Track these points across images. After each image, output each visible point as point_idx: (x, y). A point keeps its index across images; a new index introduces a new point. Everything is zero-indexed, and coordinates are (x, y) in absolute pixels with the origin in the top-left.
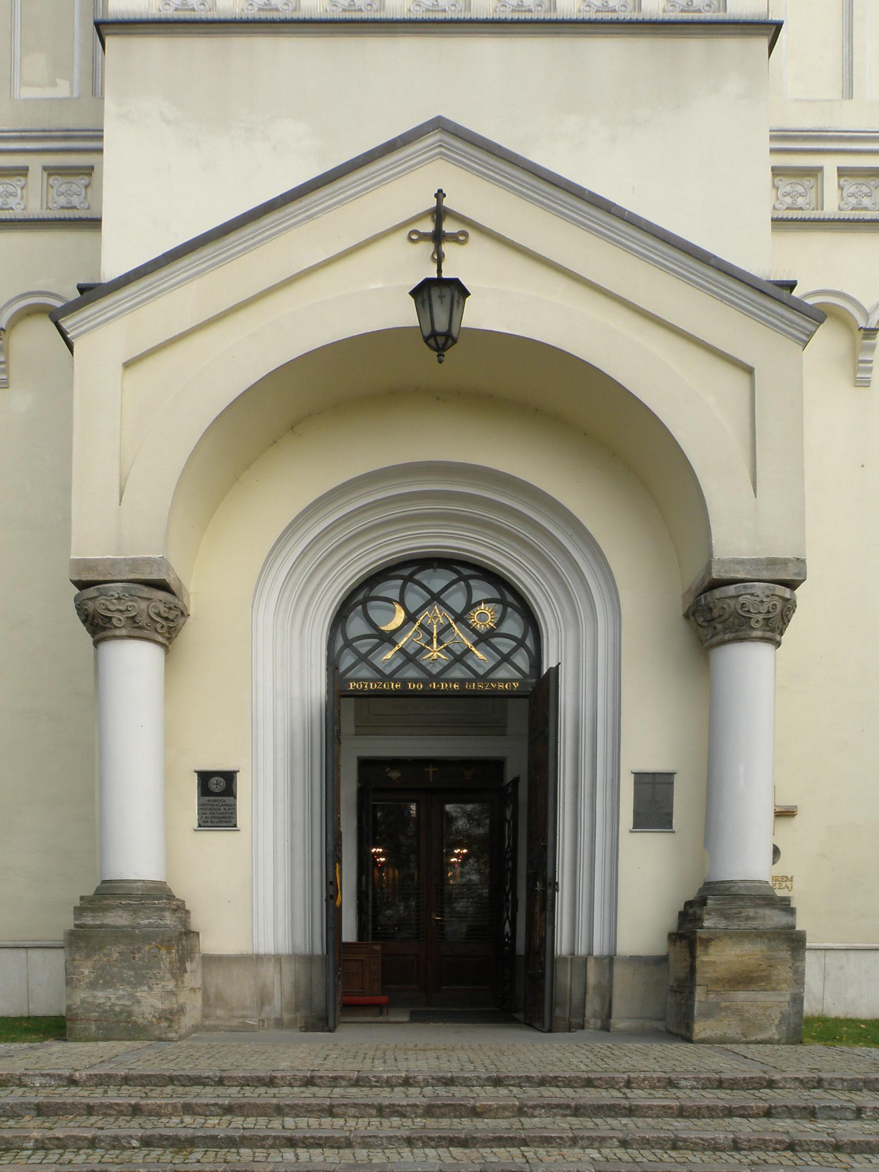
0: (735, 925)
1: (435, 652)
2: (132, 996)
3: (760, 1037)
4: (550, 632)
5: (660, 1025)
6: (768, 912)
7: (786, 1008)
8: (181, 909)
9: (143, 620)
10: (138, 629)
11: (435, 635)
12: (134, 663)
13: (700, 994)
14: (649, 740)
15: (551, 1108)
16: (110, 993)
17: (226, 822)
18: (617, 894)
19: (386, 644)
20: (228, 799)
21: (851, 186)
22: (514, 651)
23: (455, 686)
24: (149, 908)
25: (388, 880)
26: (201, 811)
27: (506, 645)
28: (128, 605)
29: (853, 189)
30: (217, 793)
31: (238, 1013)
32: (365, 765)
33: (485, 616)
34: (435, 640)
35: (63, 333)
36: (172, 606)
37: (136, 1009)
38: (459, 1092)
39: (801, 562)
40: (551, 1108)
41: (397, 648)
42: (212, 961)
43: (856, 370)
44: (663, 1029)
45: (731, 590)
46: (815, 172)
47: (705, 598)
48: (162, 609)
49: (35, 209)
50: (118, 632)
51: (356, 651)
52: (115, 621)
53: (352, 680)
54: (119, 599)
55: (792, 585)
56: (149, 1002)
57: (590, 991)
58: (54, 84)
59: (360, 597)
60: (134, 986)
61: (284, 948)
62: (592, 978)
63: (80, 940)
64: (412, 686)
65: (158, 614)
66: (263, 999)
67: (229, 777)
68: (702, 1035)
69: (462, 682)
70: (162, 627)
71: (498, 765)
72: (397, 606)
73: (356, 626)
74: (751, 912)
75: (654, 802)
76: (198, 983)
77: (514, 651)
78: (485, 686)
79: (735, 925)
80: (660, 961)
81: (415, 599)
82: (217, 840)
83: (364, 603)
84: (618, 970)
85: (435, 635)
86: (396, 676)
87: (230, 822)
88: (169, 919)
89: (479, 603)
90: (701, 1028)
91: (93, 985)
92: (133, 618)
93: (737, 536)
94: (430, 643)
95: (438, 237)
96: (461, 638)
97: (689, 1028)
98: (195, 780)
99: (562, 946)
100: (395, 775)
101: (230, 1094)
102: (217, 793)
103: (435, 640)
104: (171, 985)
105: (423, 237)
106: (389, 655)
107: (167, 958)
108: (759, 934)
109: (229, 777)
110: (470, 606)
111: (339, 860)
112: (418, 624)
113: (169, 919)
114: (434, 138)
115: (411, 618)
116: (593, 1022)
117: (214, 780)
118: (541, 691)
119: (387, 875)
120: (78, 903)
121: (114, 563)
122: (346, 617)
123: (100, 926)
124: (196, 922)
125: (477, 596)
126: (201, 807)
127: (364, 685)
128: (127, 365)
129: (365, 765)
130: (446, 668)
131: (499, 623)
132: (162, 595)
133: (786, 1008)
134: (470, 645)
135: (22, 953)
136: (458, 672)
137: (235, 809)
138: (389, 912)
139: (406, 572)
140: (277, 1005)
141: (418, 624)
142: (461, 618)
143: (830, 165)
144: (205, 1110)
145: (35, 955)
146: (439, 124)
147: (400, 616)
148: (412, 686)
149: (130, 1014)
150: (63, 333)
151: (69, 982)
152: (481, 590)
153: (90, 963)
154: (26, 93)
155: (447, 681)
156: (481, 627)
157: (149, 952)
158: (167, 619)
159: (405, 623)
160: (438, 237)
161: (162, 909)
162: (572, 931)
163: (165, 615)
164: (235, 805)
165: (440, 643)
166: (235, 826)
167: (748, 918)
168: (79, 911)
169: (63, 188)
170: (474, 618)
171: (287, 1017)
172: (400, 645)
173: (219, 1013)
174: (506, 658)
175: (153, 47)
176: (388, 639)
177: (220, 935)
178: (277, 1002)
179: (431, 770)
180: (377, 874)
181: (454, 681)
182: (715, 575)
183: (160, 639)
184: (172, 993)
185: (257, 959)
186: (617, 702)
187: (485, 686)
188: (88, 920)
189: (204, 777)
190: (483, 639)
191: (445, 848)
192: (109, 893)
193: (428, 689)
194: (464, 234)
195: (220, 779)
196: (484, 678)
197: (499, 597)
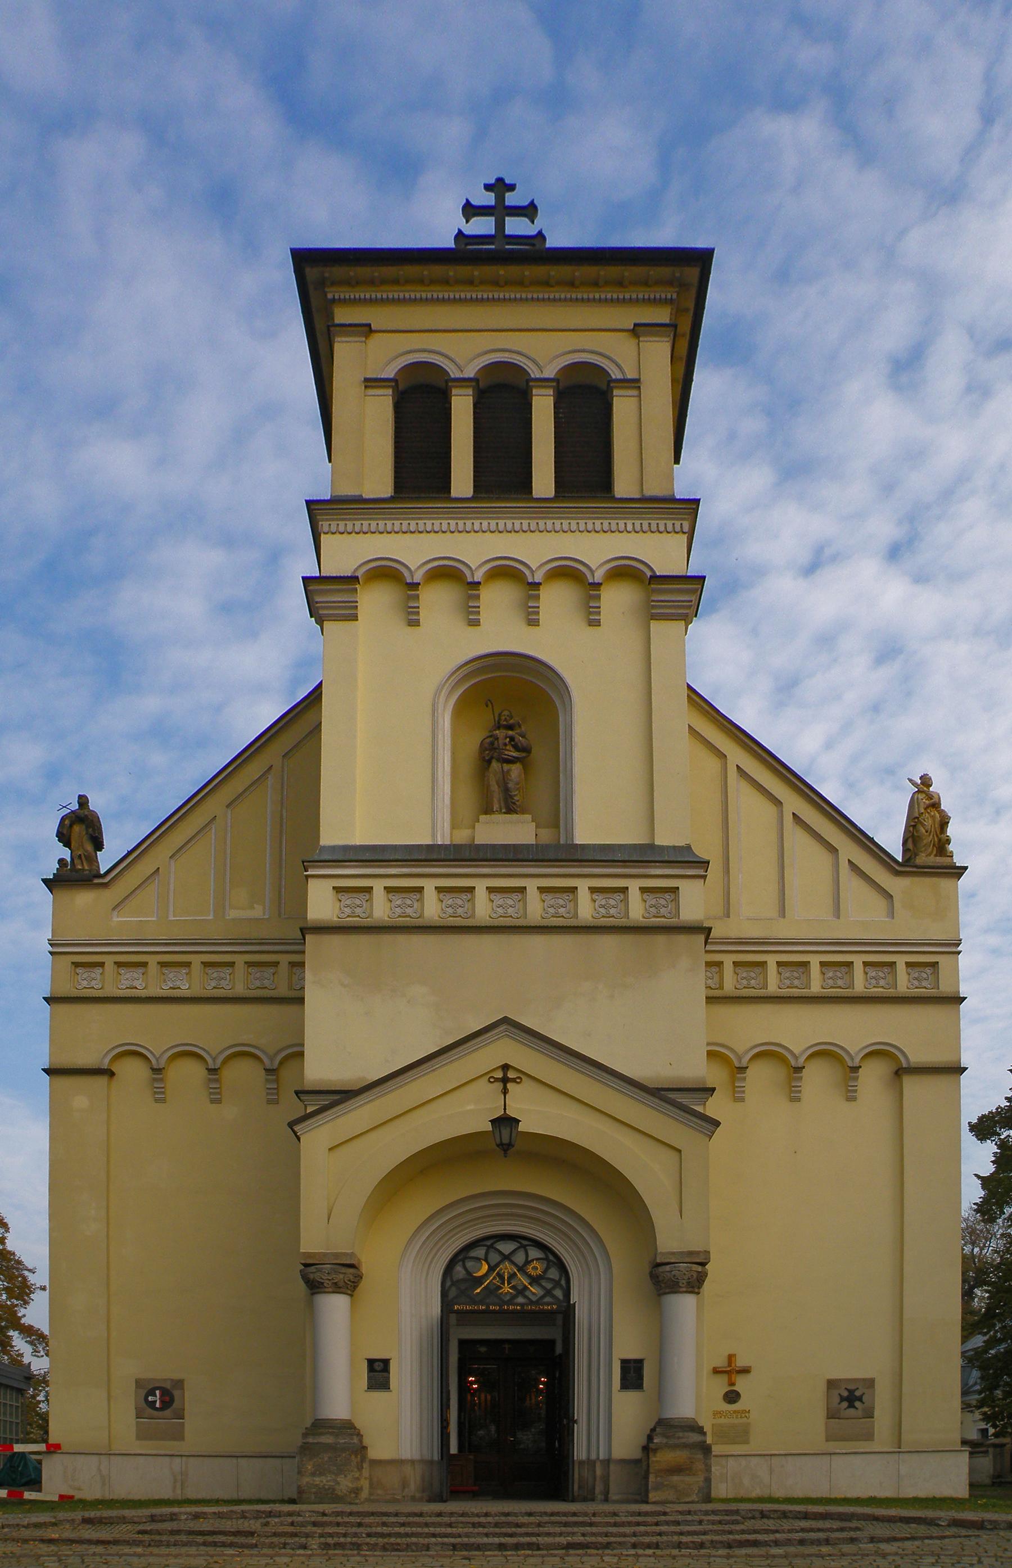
0: (671, 1442)
1: (506, 1288)
2: (335, 1481)
3: (687, 1500)
6: (691, 1434)
7: (701, 1484)
8: (359, 1435)
9: (341, 1284)
10: (338, 1288)
12: (335, 1306)
13: (652, 1478)
14: (627, 1344)
15: (553, 1523)
16: (324, 1479)
18: (609, 1424)
20: (385, 1374)
21: (787, 973)
22: (553, 1288)
25: (480, 1403)
28: (331, 1275)
29: (788, 975)
30: (378, 1373)
32: (462, 1343)
33: (536, 1268)
35: (295, 1133)
37: (337, 1487)
38: (510, 1519)
39: (707, 1253)
40: (553, 1523)
42: (376, 1463)
43: (791, 1092)
45: (668, 1268)
48: (352, 1277)
49: (240, 990)
55: (703, 1264)
56: (345, 1484)
57: (598, 1479)
58: (252, 908)
61: (417, 1456)
62: (599, 1472)
63: (306, 1449)
66: (404, 1484)
67: (386, 1362)
68: (654, 1500)
69: (522, 1305)
71: (552, 1343)
73: (459, 1271)
74: (681, 1434)
75: (632, 1374)
76: (367, 1475)
79: (671, 1442)
80: (637, 1462)
81: (495, 1258)
82: (379, 1396)
83: (463, 1261)
84: (612, 1467)
88: (356, 1440)
89: (533, 1260)
90: (653, 1496)
91: (313, 1474)
93: (671, 1238)
94: (503, 1283)
95: (505, 1080)
97: (647, 1496)
98: (365, 1365)
99: (580, 1451)
100: (483, 1349)
101: (402, 1519)
102: (378, 1373)
104: (357, 1475)
105: (497, 1080)
107: (355, 1460)
108: (685, 1446)
109: (386, 1362)
110: (528, 1262)
111: (448, 1407)
113: (356, 1440)
115: (491, 1269)
116: (600, 1497)
117: (377, 1364)
118: (567, 1312)
119: (479, 1398)
120: (304, 1431)
121: (325, 1254)
123: (317, 1443)
124: (366, 1441)
128: (330, 1149)
129: (462, 1343)
131: (545, 1271)
132: (351, 1270)
133: (701, 1484)
135: (234, 1460)
138: (481, 1432)
139: (489, 1243)
140: (413, 1487)
142: (521, 1269)
143: (771, 960)
144: (393, 1525)
145: (191, 1459)
146: (505, 1020)
147: (485, 1267)
149: (334, 1490)
150: (295, 1133)
151: (299, 1473)
152: (534, 1253)
153: (311, 1463)
154: (232, 914)
156: (533, 1273)
159: (488, 1272)
160: (505, 1080)
161: (351, 1435)
164: (389, 1378)
167: (679, 1438)
168: (305, 1435)
169: (258, 975)
170: (529, 1269)
171: (418, 1495)
173: (379, 1492)
175: (336, 941)
177: (380, 1449)
178: (412, 1487)
179: (507, 1346)
180: (469, 1397)
181: (518, 1304)
182: (658, 1261)
184: (358, 1479)
185: (401, 1462)
186: (608, 1322)
188: (310, 1440)
189: (371, 1362)
190: (535, 1280)
191: (511, 1397)
192: (320, 1425)
194: (519, 1078)
196: (537, 1303)
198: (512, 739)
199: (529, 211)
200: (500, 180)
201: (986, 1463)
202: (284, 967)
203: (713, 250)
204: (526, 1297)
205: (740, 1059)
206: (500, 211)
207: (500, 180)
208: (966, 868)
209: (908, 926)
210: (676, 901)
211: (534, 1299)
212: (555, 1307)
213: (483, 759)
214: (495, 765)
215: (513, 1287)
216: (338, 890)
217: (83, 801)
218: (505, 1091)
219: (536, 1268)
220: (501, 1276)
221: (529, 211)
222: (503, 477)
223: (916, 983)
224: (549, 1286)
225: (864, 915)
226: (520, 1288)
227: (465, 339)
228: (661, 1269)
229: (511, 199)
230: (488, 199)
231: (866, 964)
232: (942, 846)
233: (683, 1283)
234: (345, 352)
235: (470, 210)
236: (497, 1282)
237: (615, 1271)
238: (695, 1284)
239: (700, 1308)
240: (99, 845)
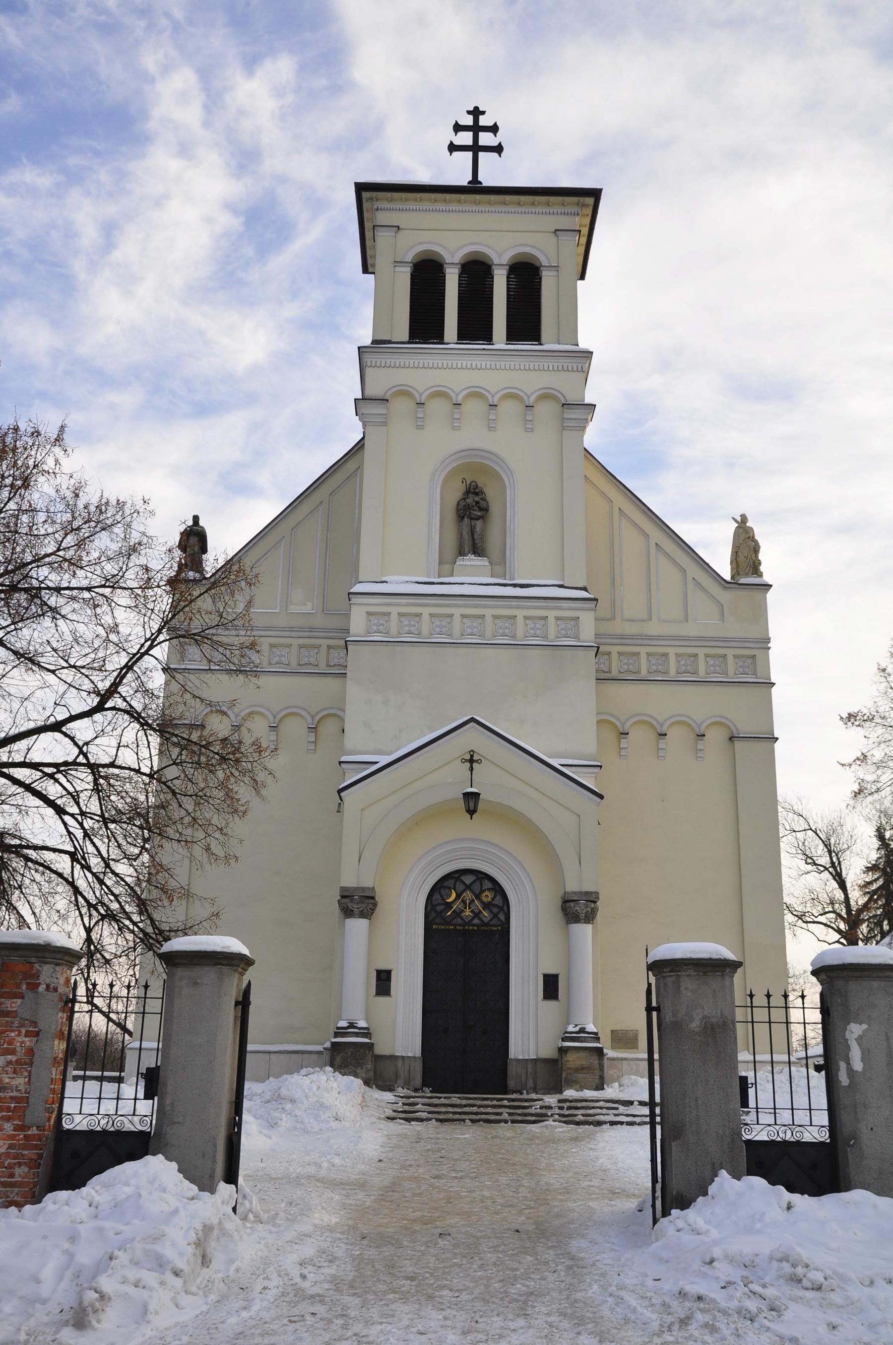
1: (468, 912)
10: (363, 915)
12: (357, 926)
28: (358, 903)
30: (383, 982)
31: (387, 1083)
33: (487, 896)
45: (572, 904)
46: (637, 654)
55: (595, 902)
58: (305, 605)
60: (356, 1067)
67: (388, 973)
82: (383, 999)
105: (466, 761)
109: (388, 973)
110: (482, 891)
114: (472, 724)
125: (485, 887)
131: (493, 899)
136: (476, 921)
142: (478, 897)
143: (643, 650)
147: (454, 895)
152: (487, 884)
154: (294, 609)
156: (485, 900)
176: (449, 906)
189: (379, 972)
190: (486, 906)
198: (477, 503)
199: (494, 129)
200: (476, 108)
202: (324, 649)
203: (601, 190)
204: (480, 919)
205: (623, 724)
206: (476, 129)
207: (476, 108)
208: (771, 586)
209: (733, 629)
210: (577, 625)
211: (486, 920)
213: (459, 515)
214: (466, 520)
215: (472, 911)
216: (369, 614)
217: (196, 519)
218: (471, 769)
219: (487, 896)
220: (464, 902)
221: (494, 129)
222: (475, 328)
223: (741, 670)
224: (495, 910)
225: (704, 620)
226: (477, 911)
227: (454, 237)
228: (568, 904)
229: (484, 121)
230: (469, 121)
231: (707, 656)
232: (755, 568)
233: (582, 916)
234: (383, 239)
235: (458, 128)
236: (461, 906)
238: (589, 918)
239: (595, 932)
240: (204, 550)
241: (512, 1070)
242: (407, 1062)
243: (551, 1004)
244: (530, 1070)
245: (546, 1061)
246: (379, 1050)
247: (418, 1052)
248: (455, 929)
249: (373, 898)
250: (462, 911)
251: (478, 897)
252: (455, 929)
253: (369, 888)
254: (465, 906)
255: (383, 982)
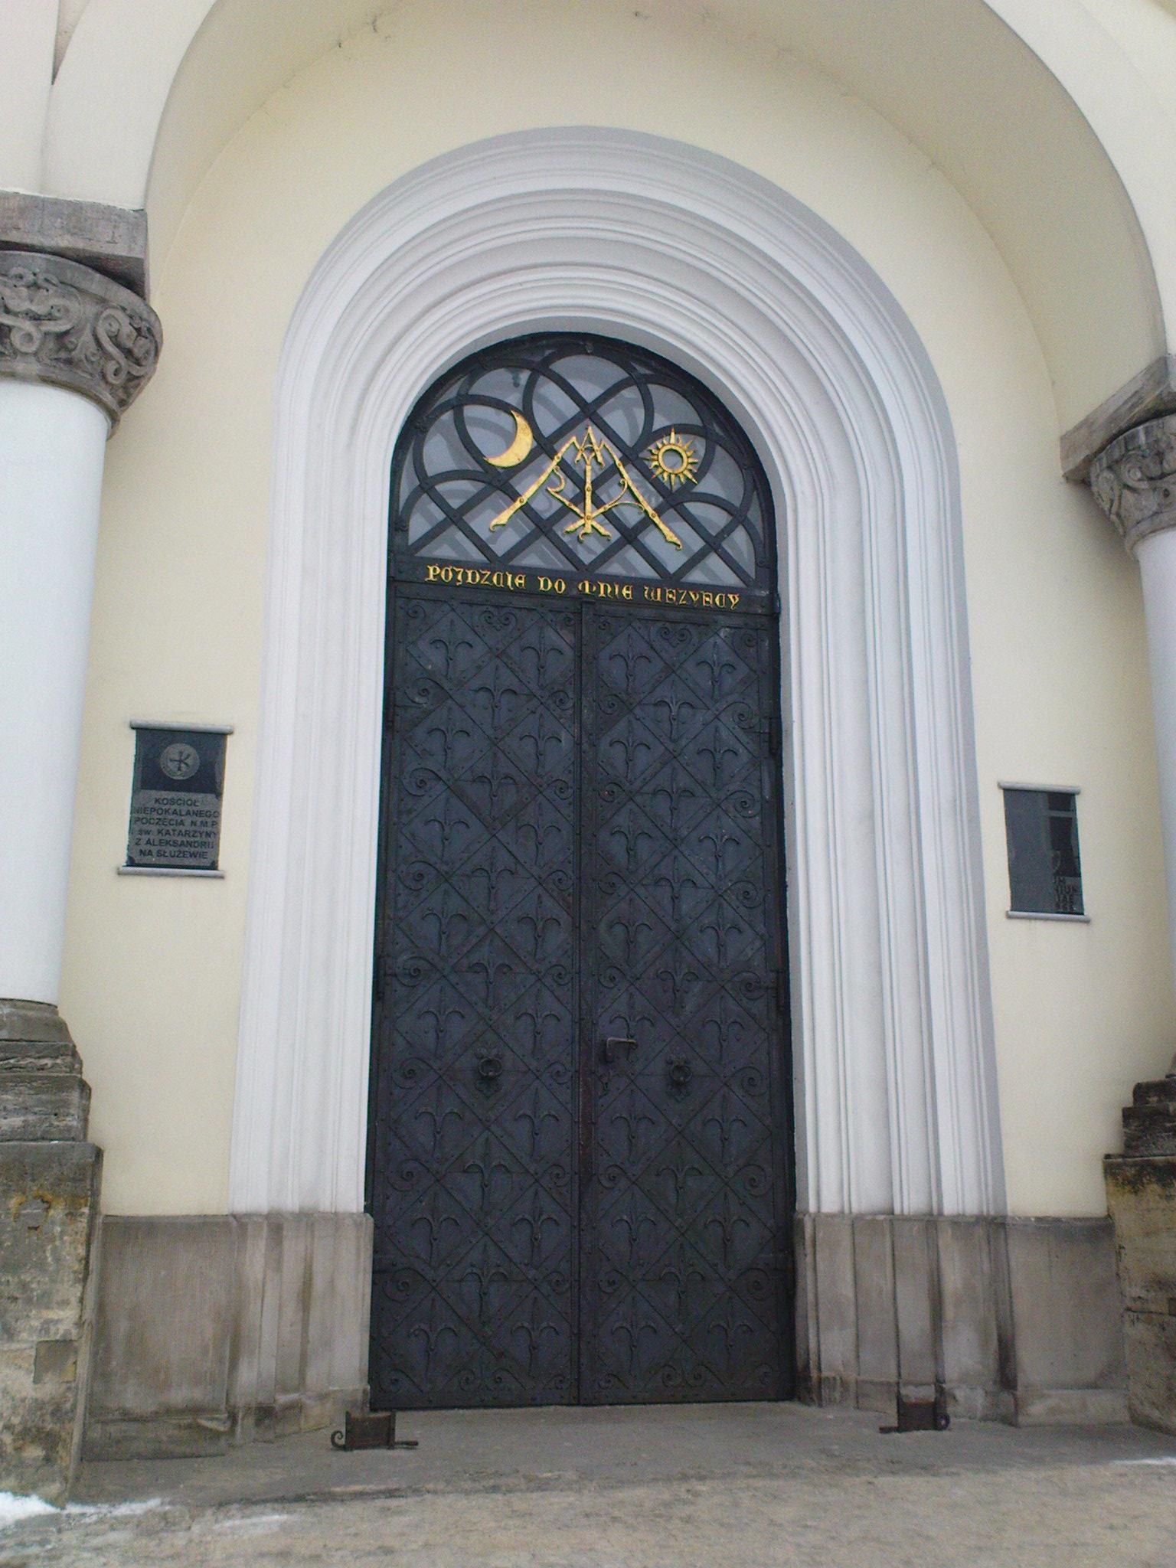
1: (589, 521)
4: (799, 497)
5: (1104, 1405)
11: (588, 485)
17: (193, 855)
19: (497, 497)
20: (202, 799)
23: (625, 592)
24: (31, 1079)
26: (138, 826)
27: (715, 518)
33: (676, 458)
34: (588, 494)
36: (144, 325)
41: (518, 504)
44: (1124, 1416)
47: (1147, 433)
50: (20, 366)
51: (440, 502)
52: (16, 338)
53: (433, 561)
54: (34, 286)
59: (451, 393)
64: (546, 586)
65: (115, 339)
67: (210, 744)
69: (637, 584)
70: (116, 373)
72: (520, 420)
73: (439, 453)
77: (727, 531)
78: (678, 596)
82: (170, 894)
83: (457, 406)
84: (1022, 1257)
85: (588, 485)
86: (515, 562)
87: (202, 855)
89: (665, 432)
92: (61, 336)
94: (579, 499)
96: (632, 496)
103: (588, 494)
106: (504, 518)
109: (210, 744)
110: (650, 436)
112: (556, 460)
115: (544, 446)
117: (173, 751)
122: (424, 431)
126: (139, 814)
127: (456, 574)
130: (604, 558)
131: (701, 472)
134: (650, 511)
137: (216, 824)
141: (556, 460)
142: (633, 456)
147: (524, 444)
148: (546, 586)
152: (671, 407)
155: (612, 580)
157: (17, 1216)
158: (128, 353)
162: (849, 1152)
163: (129, 344)
165: (597, 503)
166: (213, 866)
172: (526, 496)
174: (713, 544)
176: (500, 483)
183: (108, 398)
187: (678, 596)
189: (153, 741)
193: (574, 592)
195: (188, 749)
197: (700, 423)
201: (1134, 1125)
211: (673, 562)
212: (734, 599)
215: (610, 517)
237: (966, 455)
241: (829, 1279)
242: (293, 1248)
243: (1049, 937)
244: (953, 1279)
245: (1056, 1231)
246: (132, 1188)
247: (347, 1191)
248: (530, 591)
249: (129, 277)
250: (564, 512)
251: (633, 456)
252: (530, 591)
253: (109, 214)
254: (564, 490)
255: (176, 792)
